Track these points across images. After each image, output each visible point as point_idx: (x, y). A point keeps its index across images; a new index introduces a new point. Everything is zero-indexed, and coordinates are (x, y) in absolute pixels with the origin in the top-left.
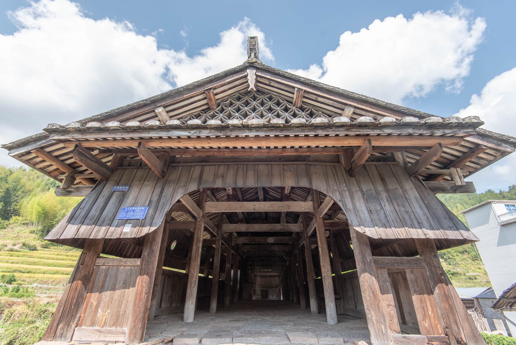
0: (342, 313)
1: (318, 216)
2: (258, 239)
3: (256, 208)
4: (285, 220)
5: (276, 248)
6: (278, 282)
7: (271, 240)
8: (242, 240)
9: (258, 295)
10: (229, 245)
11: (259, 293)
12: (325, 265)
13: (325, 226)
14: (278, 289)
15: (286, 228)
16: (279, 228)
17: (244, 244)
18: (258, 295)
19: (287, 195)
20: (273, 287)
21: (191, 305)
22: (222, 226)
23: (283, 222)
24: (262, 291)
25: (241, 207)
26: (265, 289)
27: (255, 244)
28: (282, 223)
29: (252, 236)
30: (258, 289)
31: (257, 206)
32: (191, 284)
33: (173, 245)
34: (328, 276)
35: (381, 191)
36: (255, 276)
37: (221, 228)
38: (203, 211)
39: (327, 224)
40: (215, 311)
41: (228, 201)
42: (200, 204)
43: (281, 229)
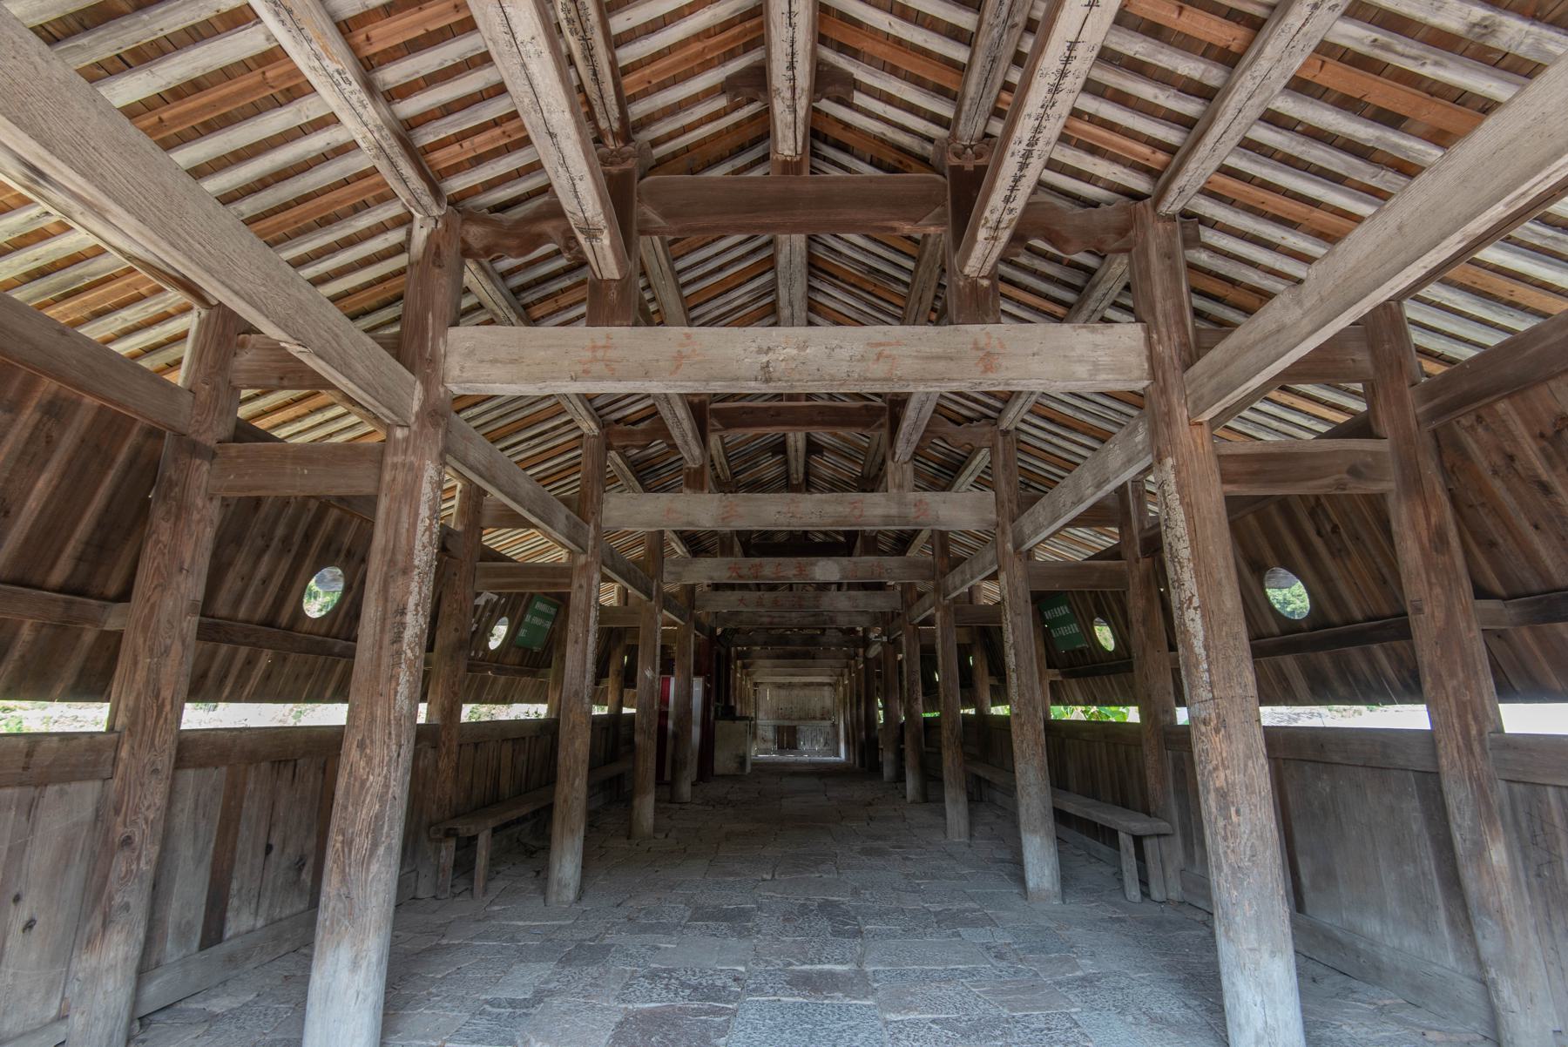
0: (1173, 895)
1: (1182, 414)
2: (770, 568)
3: (779, 368)
4: (909, 474)
5: (840, 602)
6: (828, 703)
7: (827, 569)
8: (706, 571)
9: (764, 740)
10: (649, 594)
11: (770, 735)
12: (1232, 721)
13: (1226, 479)
14: (828, 723)
15: (912, 512)
16: (879, 511)
17: (717, 587)
18: (764, 740)
19: (974, 285)
20: (814, 718)
21: (344, 975)
22: (600, 502)
23: (900, 486)
24: (779, 730)
25: (680, 357)
26: (786, 723)
27: (758, 587)
28: (893, 491)
29: (746, 554)
30: (766, 725)
31: (782, 353)
32: (347, 843)
33: (319, 600)
34: (1249, 789)
35: (801, 568)
36: (756, 684)
37: (598, 512)
38: (426, 383)
39: (1233, 467)
40: (570, 894)
41: (592, 322)
42: (410, 349)
43: (887, 519)
